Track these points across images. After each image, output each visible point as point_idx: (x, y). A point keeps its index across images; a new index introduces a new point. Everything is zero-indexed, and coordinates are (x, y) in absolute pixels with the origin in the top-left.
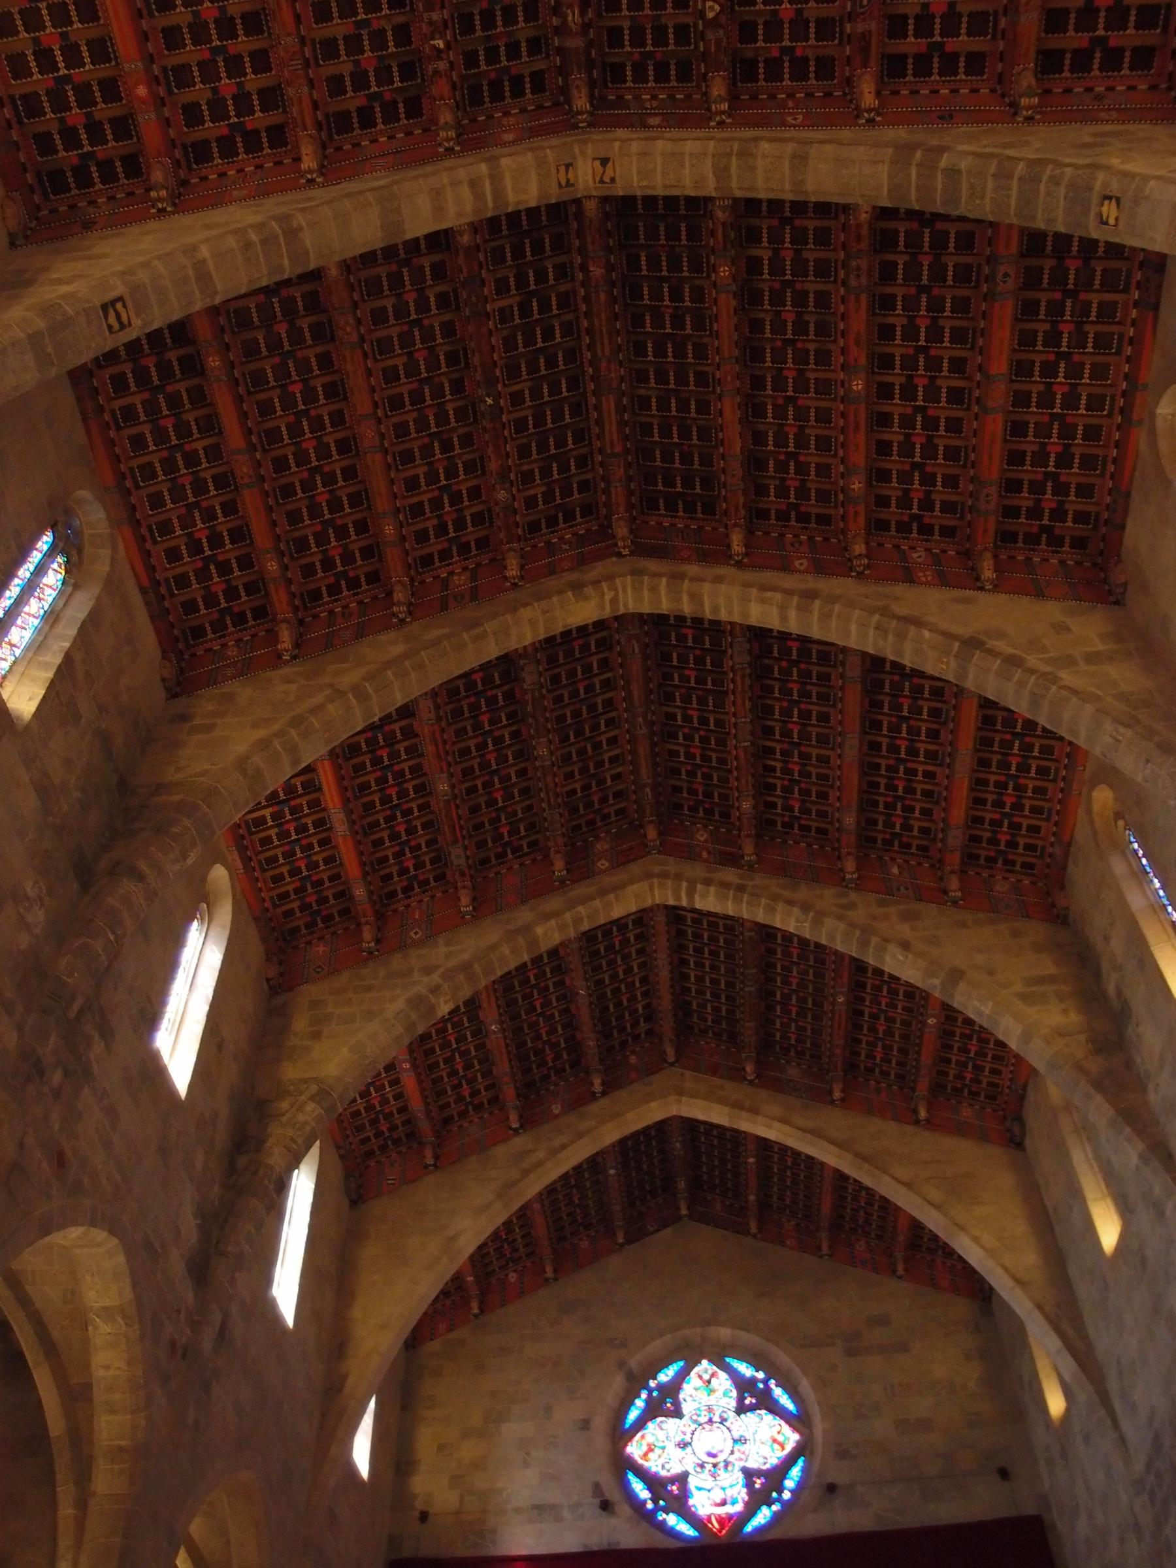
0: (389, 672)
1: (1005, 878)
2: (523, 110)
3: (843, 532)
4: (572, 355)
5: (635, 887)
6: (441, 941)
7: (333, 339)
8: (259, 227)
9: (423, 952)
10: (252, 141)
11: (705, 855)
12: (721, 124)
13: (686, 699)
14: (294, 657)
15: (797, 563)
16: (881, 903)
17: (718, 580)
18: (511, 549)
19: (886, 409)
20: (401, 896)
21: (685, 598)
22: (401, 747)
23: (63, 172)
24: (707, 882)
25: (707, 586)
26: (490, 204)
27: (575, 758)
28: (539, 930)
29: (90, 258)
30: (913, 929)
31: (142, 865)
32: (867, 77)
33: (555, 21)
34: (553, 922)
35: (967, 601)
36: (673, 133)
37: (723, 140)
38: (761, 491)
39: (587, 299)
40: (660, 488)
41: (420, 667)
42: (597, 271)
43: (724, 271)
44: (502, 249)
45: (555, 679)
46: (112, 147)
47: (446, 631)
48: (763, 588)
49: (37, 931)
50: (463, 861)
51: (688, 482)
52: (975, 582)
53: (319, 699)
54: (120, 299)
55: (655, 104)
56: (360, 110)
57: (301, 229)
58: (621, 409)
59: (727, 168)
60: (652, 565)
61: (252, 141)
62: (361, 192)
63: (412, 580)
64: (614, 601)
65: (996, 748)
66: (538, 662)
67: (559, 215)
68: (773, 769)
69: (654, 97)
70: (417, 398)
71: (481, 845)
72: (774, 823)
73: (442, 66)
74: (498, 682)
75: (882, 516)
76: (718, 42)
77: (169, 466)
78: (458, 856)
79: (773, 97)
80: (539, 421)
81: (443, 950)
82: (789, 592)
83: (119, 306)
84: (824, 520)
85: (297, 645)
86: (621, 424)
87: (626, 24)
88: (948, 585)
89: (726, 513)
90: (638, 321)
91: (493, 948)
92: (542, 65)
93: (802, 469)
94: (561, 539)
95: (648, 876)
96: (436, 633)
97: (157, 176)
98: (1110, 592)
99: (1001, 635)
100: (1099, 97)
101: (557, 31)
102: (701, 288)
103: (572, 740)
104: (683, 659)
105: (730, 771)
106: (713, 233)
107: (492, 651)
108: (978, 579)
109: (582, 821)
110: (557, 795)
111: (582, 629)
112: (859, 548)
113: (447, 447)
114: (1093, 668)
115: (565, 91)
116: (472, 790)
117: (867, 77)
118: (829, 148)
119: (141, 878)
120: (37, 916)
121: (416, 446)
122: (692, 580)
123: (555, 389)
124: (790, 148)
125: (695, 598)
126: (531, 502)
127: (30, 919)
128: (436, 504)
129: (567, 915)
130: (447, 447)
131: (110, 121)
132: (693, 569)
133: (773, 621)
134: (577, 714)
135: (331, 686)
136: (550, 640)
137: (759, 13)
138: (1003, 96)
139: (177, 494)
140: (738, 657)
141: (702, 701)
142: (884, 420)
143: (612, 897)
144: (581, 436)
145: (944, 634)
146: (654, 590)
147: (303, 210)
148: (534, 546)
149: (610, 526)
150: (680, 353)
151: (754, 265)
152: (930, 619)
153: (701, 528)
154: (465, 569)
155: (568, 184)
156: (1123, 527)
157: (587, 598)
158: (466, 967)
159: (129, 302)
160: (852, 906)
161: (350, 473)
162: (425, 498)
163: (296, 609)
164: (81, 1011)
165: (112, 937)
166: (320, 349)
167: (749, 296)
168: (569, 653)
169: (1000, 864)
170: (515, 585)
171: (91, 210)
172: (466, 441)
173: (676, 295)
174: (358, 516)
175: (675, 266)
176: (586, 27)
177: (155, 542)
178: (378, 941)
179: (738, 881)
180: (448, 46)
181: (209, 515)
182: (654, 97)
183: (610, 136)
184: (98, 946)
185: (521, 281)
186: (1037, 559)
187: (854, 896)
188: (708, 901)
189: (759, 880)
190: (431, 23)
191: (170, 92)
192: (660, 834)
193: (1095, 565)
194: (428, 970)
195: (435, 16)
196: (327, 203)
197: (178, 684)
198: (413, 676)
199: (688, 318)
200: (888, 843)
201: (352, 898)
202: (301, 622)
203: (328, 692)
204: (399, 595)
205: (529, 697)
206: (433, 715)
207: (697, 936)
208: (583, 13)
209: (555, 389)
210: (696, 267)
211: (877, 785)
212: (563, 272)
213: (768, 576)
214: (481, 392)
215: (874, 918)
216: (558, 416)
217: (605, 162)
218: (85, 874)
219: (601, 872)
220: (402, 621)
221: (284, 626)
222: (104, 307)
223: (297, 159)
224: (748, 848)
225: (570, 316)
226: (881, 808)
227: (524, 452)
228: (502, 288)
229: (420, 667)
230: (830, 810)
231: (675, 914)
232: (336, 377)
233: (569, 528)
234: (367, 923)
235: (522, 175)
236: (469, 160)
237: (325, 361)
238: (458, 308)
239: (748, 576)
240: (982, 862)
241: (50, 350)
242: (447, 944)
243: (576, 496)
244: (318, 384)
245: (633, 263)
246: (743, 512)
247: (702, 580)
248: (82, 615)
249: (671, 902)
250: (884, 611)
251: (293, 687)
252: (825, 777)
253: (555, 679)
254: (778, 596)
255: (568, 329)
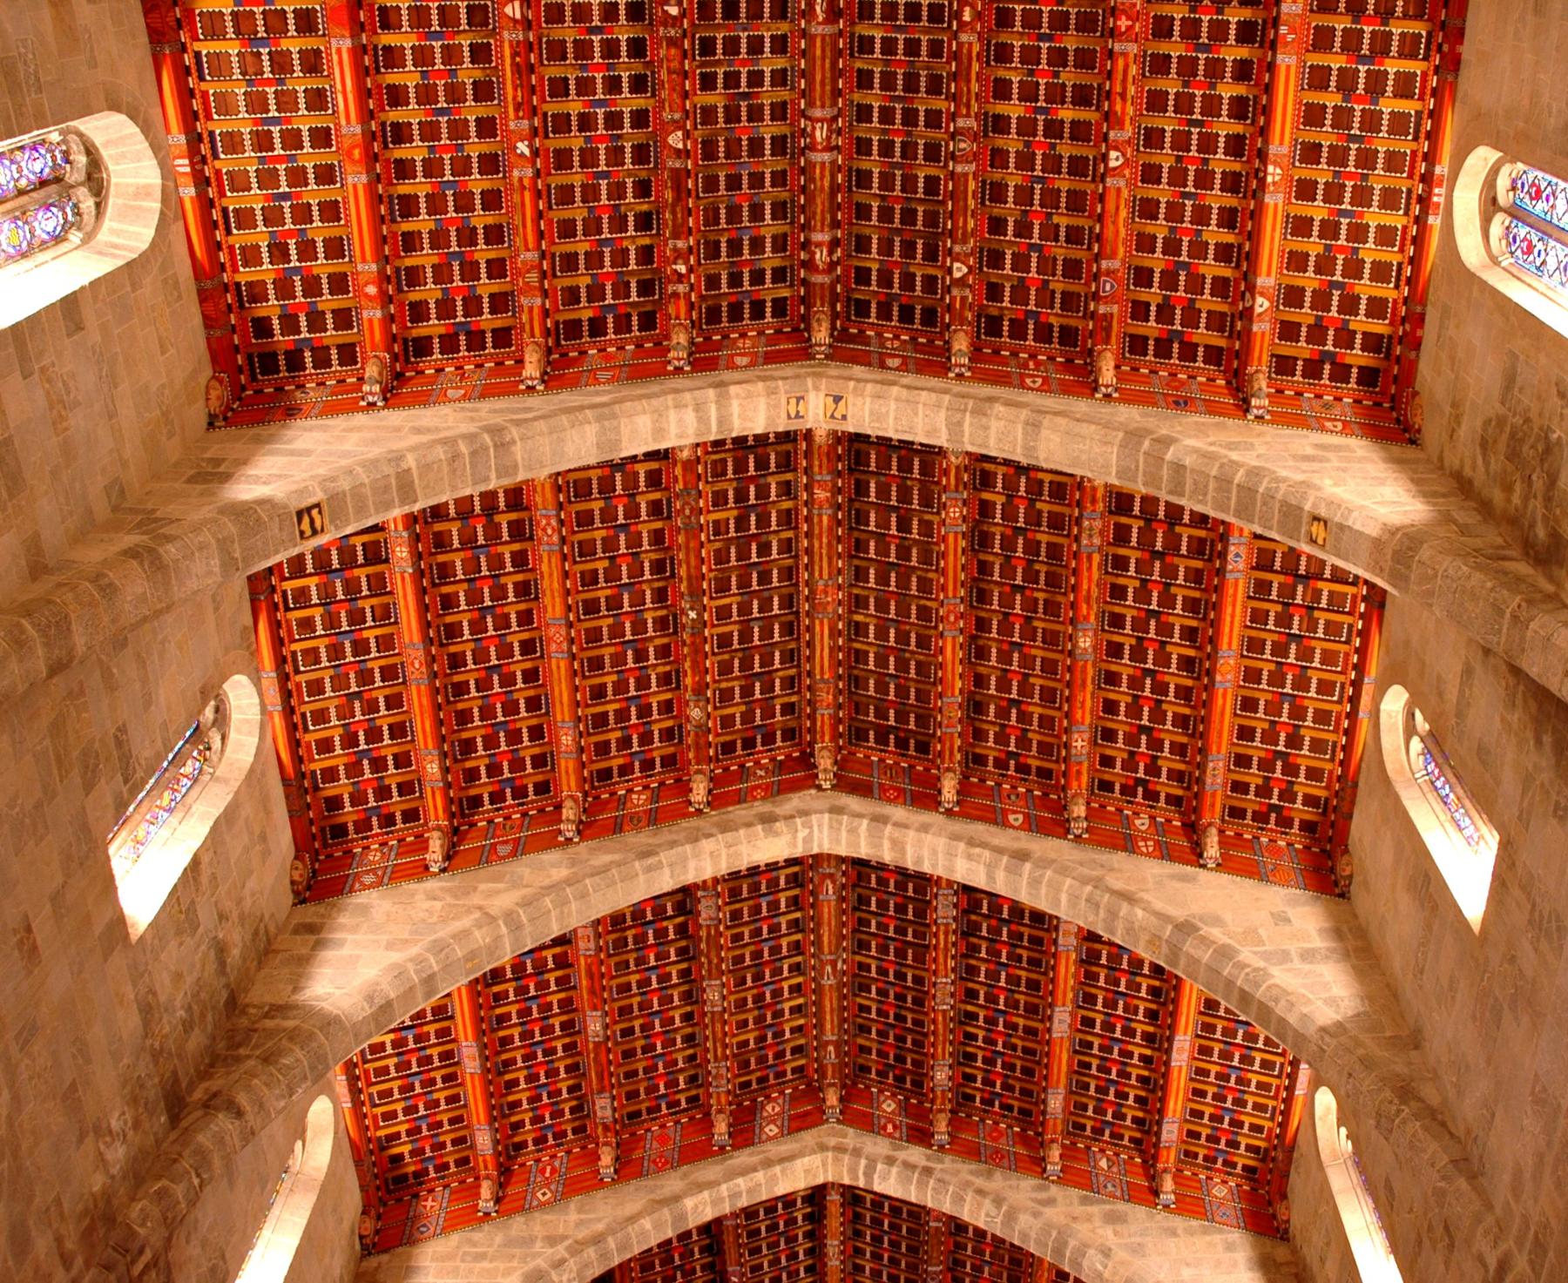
0: (547, 900)
1: (1224, 1182)
2: (761, 333)
3: (1064, 789)
4: (789, 574)
5: (806, 1159)
6: (572, 1206)
7: (531, 538)
8: (471, 438)
9: (548, 1217)
10: (476, 340)
11: (890, 1128)
12: (960, 376)
13: (883, 949)
14: (443, 870)
15: (1011, 817)
16: (1084, 1201)
17: (924, 828)
18: (698, 772)
19: (1114, 668)
20: (531, 1148)
21: (886, 844)
22: (552, 977)
23: (275, 355)
24: (890, 1161)
25: (911, 833)
26: (714, 428)
27: (750, 1005)
28: (689, 1203)
29: (292, 453)
30: (1116, 1233)
31: (242, 1099)
32: (1109, 355)
33: (803, 255)
34: (706, 1194)
35: (1184, 878)
36: (909, 379)
37: (957, 395)
38: (980, 735)
39: (808, 519)
40: (871, 718)
41: (583, 896)
42: (821, 494)
43: (955, 512)
44: (724, 461)
45: (736, 915)
46: (331, 335)
47: (617, 857)
48: (971, 843)
49: (115, 1171)
50: (609, 1112)
51: (902, 717)
52: (1195, 856)
53: (466, 922)
54: (318, 505)
55: (896, 344)
56: (581, 116)
57: (513, 442)
58: (835, 634)
59: (960, 423)
60: (853, 802)
61: (476, 340)
62: (582, 408)
63: (586, 794)
64: (808, 840)
65: (1218, 1036)
66: (718, 895)
67: (786, 447)
68: (974, 1037)
69: (897, 337)
70: (614, 603)
71: (633, 1095)
72: (972, 1098)
73: (681, 288)
74: (670, 912)
75: (1106, 777)
76: (964, 299)
77: (336, 652)
78: (603, 1108)
79: (1015, 354)
80: (746, 636)
81: (573, 1216)
82: (999, 851)
83: (315, 512)
84: (1044, 773)
85: (448, 857)
86: (834, 649)
87: (875, 266)
88: (1172, 859)
89: (940, 754)
90: (860, 546)
91: (632, 1219)
92: (786, 293)
93: (1024, 717)
94: (757, 763)
95: (823, 1148)
96: (607, 858)
97: (372, 370)
98: (1336, 883)
99: (1217, 921)
100: (1326, 406)
101: (804, 264)
102: (930, 523)
103: (749, 983)
104: (882, 905)
105: (926, 1035)
106: (946, 472)
107: (666, 882)
108: (1201, 855)
109: (753, 1077)
110: (725, 1046)
111: (773, 867)
112: (1079, 810)
113: (641, 656)
114: (1307, 967)
115: (806, 319)
116: (628, 1032)
117: (1109, 355)
118: (1062, 421)
119: (239, 1114)
120: (118, 1154)
121: (607, 652)
122: (896, 824)
123: (765, 606)
124: (1024, 414)
125: (897, 845)
126: (727, 721)
127: (109, 1156)
128: (622, 715)
129: (724, 1187)
130: (641, 656)
131: (339, 347)
132: (898, 812)
133: (979, 880)
134: (757, 955)
135: (480, 908)
136: (735, 876)
137: (1008, 277)
138: (1238, 389)
139: (339, 682)
140: (945, 911)
141: (900, 953)
142: (1112, 679)
143: (777, 1169)
144: (790, 657)
145: (1158, 915)
146: (853, 831)
147: (518, 423)
148: (726, 769)
149: (812, 755)
150: (903, 583)
151: (986, 509)
152: (1145, 896)
153: (912, 767)
154: (646, 787)
155: (798, 416)
156: (1350, 816)
157: (777, 834)
158: (598, 1240)
159: (325, 508)
160: (1050, 1202)
161: (530, 676)
162: (611, 708)
163: (452, 816)
164: (147, 1268)
165: (196, 1181)
166: (516, 547)
167: (979, 539)
168: (755, 888)
169: (1219, 1165)
170: (699, 812)
171: (298, 394)
172: (663, 652)
173: (904, 526)
174: (534, 722)
175: (905, 496)
176: (832, 266)
177: (306, 730)
178: (498, 1201)
179: (924, 1163)
180: (691, 270)
181: (371, 707)
182: (897, 337)
183: (846, 373)
184: (179, 1191)
185: (741, 496)
186: (1264, 840)
187: (1054, 1190)
188: (889, 1184)
189: (949, 1163)
190: (675, 249)
191: (399, 290)
192: (841, 1099)
193: (1323, 851)
194: (552, 1241)
195: (680, 244)
196: (543, 417)
197: (309, 888)
198: (574, 906)
199: (914, 551)
200: (1098, 1131)
201: (473, 1147)
202: (456, 831)
203: (477, 915)
204: (569, 812)
205: (703, 933)
206: (592, 945)
207: (877, 1222)
208: (830, 253)
209: (765, 606)
210: (926, 501)
211: (1088, 1066)
212: (787, 489)
213: (979, 829)
214: (685, 605)
215: (1075, 1219)
216: (767, 633)
217: (837, 399)
218: (176, 1104)
219: (770, 1139)
220: (569, 840)
221: (436, 834)
222: (300, 514)
223: (520, 362)
224: (941, 1126)
225: (790, 534)
226: (1092, 1092)
227: (725, 669)
228: (719, 500)
229: (583, 896)
230: (1035, 1088)
231: (852, 1196)
232: (529, 576)
233: (767, 756)
234: (487, 1177)
235: (752, 405)
236: (698, 383)
237: (520, 560)
238: (669, 517)
239: (959, 826)
240: (1200, 1160)
241: (237, 555)
242: (580, 1211)
243: (778, 718)
244: (509, 583)
245: (862, 489)
246: (958, 757)
247: (906, 826)
248: (216, 812)
249: (847, 1181)
250: (1097, 883)
251: (438, 905)
252: (1032, 1052)
253: (736, 915)
254: (987, 853)
255: (786, 546)
